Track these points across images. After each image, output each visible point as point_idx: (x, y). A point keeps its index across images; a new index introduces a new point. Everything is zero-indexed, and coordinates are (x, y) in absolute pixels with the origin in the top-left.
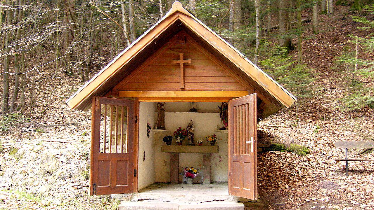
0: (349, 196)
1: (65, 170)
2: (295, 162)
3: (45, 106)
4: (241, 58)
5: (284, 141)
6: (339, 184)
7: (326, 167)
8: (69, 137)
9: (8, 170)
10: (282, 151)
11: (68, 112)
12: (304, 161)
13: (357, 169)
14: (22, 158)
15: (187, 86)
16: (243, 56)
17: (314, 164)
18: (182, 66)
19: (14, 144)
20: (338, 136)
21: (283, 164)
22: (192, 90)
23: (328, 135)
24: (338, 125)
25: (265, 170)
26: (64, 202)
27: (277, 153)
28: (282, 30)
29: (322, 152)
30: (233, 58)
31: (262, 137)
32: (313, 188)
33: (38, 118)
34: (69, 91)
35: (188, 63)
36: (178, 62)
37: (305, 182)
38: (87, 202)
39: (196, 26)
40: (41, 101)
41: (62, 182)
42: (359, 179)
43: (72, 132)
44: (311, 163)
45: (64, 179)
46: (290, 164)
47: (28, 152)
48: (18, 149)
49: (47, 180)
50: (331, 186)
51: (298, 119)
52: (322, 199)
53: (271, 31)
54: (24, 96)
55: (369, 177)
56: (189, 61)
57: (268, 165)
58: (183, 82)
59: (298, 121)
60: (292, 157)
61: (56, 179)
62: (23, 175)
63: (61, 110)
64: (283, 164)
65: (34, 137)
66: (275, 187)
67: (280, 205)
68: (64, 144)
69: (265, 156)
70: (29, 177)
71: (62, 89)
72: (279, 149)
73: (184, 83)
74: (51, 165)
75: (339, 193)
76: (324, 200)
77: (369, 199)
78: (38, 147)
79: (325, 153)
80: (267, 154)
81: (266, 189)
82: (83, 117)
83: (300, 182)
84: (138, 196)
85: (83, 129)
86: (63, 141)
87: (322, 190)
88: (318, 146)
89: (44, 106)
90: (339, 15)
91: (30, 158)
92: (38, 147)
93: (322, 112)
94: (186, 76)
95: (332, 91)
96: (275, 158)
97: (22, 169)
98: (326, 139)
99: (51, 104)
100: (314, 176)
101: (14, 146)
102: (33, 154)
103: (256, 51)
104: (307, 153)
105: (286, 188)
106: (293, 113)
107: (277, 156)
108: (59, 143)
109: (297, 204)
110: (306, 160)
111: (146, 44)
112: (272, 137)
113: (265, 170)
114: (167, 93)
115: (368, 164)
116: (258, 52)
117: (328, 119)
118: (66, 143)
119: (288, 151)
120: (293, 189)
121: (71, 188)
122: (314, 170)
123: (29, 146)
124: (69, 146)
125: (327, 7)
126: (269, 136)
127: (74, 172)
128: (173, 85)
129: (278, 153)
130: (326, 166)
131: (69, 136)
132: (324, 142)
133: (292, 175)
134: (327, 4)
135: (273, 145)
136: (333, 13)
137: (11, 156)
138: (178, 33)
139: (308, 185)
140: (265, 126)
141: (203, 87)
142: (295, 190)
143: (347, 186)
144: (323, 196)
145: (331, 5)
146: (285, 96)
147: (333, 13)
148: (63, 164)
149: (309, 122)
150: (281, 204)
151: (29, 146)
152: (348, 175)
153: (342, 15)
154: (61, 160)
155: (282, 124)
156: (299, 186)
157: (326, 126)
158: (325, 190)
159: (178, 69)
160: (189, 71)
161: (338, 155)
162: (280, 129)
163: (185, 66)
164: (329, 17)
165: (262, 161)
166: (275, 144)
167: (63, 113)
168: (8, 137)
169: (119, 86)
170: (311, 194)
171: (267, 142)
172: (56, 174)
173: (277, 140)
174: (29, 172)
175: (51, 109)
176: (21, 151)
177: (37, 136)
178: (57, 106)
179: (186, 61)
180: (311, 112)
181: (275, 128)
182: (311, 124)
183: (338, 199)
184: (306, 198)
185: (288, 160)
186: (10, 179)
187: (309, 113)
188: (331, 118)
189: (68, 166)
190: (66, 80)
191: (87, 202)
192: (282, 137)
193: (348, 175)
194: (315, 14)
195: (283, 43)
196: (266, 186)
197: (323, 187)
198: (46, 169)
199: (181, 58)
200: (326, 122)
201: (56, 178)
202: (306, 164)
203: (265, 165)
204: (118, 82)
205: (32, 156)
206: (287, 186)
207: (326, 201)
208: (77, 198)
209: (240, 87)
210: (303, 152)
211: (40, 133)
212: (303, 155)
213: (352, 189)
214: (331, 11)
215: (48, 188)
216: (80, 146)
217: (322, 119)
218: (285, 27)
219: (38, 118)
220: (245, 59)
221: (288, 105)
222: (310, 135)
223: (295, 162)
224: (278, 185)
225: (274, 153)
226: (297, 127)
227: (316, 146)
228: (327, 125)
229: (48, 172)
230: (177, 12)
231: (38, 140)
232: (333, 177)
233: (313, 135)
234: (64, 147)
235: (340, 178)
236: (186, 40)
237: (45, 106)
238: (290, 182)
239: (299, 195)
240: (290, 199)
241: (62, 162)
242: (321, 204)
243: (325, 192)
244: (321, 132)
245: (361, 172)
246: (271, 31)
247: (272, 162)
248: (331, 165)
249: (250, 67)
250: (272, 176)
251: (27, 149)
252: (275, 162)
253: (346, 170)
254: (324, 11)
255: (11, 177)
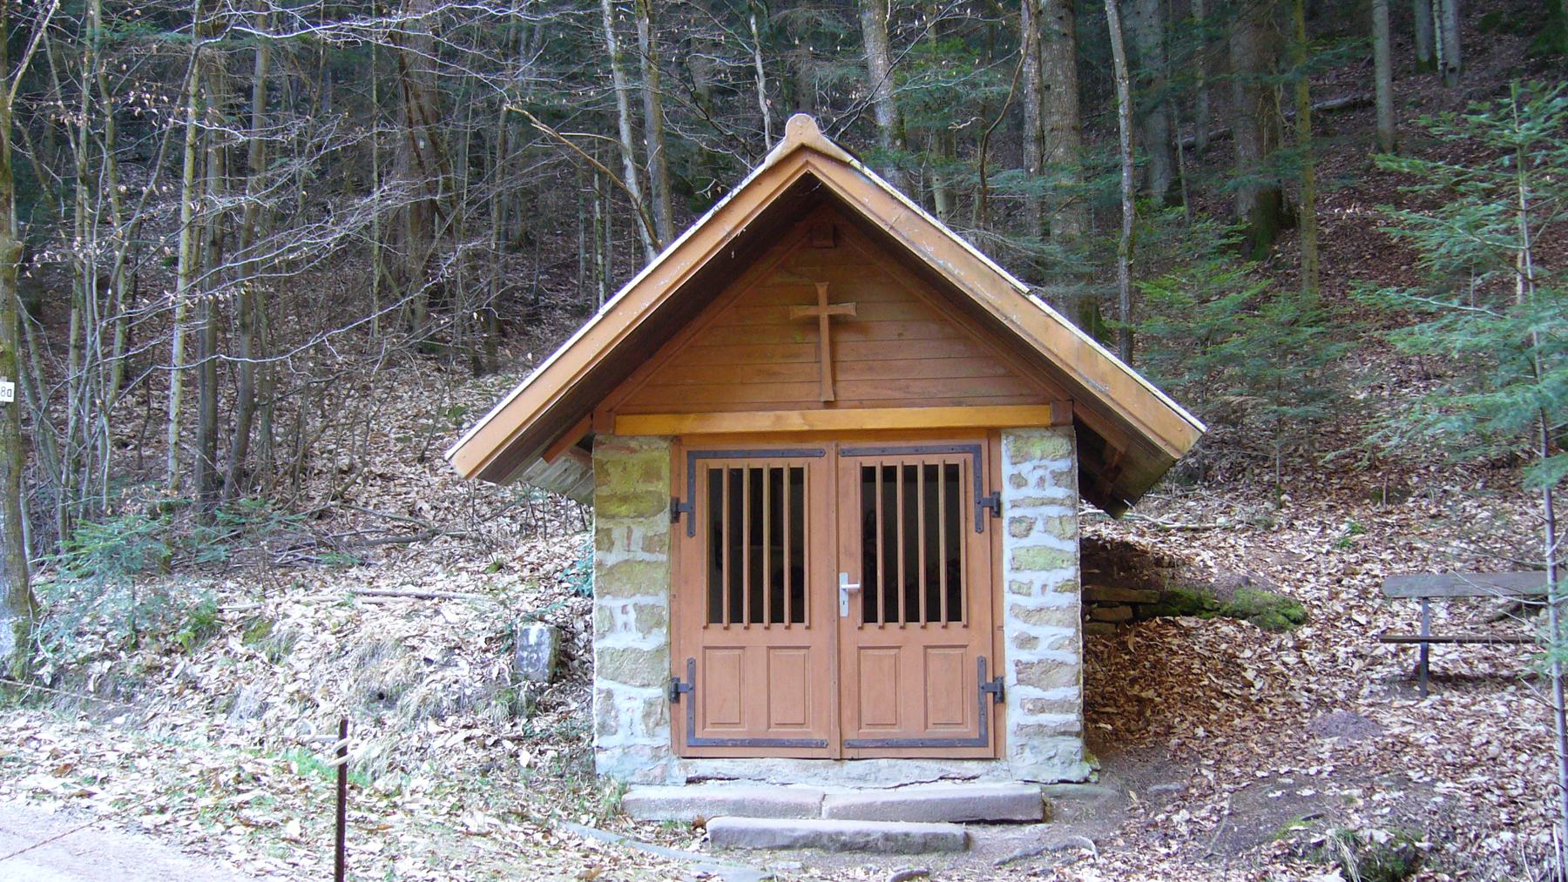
0: (1405, 759)
1: (440, 687)
2: (1248, 653)
3: (345, 472)
4: (1016, 296)
5: (1212, 580)
6: (1385, 722)
7: (1355, 669)
8: (440, 581)
9: (248, 691)
10: (1205, 614)
11: (428, 491)
12: (1280, 647)
13: (1465, 670)
14: (288, 650)
15: (843, 395)
16: (1024, 288)
17: (1313, 659)
18: (824, 325)
19: (256, 604)
20: (1425, 559)
21: (1204, 660)
22: (861, 404)
23: (1387, 556)
24: (1433, 517)
25: (1133, 681)
26: (447, 784)
27: (1184, 624)
28: (1245, 149)
29: (1355, 617)
30: (989, 296)
31: (1130, 568)
32: (1290, 737)
33: (321, 516)
34: (428, 415)
35: (845, 316)
36: (812, 311)
37: (1269, 716)
38: (520, 784)
39: (869, 192)
40: (330, 452)
41: (433, 727)
42: (1464, 706)
43: (448, 561)
44: (1305, 655)
45: (439, 717)
46: (1230, 659)
47: (308, 630)
48: (272, 622)
49: (379, 722)
50: (1351, 728)
51: (1284, 497)
52: (1312, 771)
53: (1208, 150)
54: (269, 439)
55: (1500, 699)
56: (847, 309)
57: (1148, 664)
58: (830, 381)
59: (1281, 505)
60: (1240, 636)
61: (411, 714)
62: (297, 708)
63: (404, 485)
64: (1204, 660)
65: (318, 584)
66: (1157, 734)
67: (1167, 791)
68: (428, 603)
69: (1139, 634)
70: (320, 711)
71: (399, 406)
72: (1195, 607)
73: (834, 382)
74: (392, 670)
75: (1372, 749)
76: (1319, 772)
77: (1473, 766)
78: (342, 614)
79: (1362, 620)
80: (1147, 628)
81: (1126, 744)
82: (485, 510)
83: (1250, 716)
84: (686, 767)
85: (490, 550)
86: (424, 591)
87: (1319, 741)
88: (1343, 596)
89: (342, 472)
90: (1484, 74)
91: (317, 651)
92: (342, 614)
93: (1377, 469)
94: (841, 357)
95: (1425, 388)
96: (1176, 641)
97: (294, 687)
98: (1377, 569)
99: (366, 464)
100: (1303, 698)
101: (257, 613)
102: (326, 637)
103: (1123, 247)
104: (1298, 622)
105: (1195, 737)
106: (1266, 478)
107: (1186, 633)
108: (411, 600)
109: (1225, 786)
110: (1291, 644)
111: (698, 263)
112: (1171, 565)
113: (1133, 681)
114: (779, 418)
115: (1514, 654)
116: (1131, 251)
117: (1397, 495)
118: (436, 600)
119: (1225, 614)
120: (1220, 740)
121: (462, 746)
122: (1312, 679)
123: (310, 611)
124: (445, 608)
125: (1439, 46)
126: (1159, 562)
127: (468, 692)
128: (797, 392)
129: (1186, 622)
130: (1358, 664)
131: (441, 576)
132: (1368, 581)
133: (1227, 696)
134: (1438, 32)
135: (1174, 596)
136: (1463, 69)
137: (251, 646)
138: (809, 213)
139: (1275, 726)
140: (1155, 525)
141: (898, 395)
142: (1225, 744)
143: (1408, 728)
144: (1318, 759)
145: (1451, 37)
146: (1167, 419)
147: (1463, 69)
148: (431, 668)
149: (1324, 507)
150: (1171, 787)
151: (310, 611)
152: (1426, 694)
153: (1497, 78)
154: (423, 653)
155: (1222, 520)
156: (1244, 729)
157: (1386, 524)
158: (1328, 743)
159: (812, 338)
160: (848, 340)
161: (1410, 625)
162: (1205, 538)
163: (836, 323)
164: (1445, 86)
165: (1129, 653)
166: (1177, 590)
167: (413, 495)
168: (229, 584)
169: (615, 399)
170: (1279, 754)
171: (1148, 584)
172: (412, 698)
173: (1188, 575)
174: (317, 696)
175: (366, 479)
176: (282, 628)
177: (329, 578)
178: (388, 471)
179: (838, 310)
180: (1336, 472)
181: (1189, 534)
182: (1329, 519)
183: (1368, 768)
184: (1258, 768)
185: (1224, 646)
186: (254, 721)
187: (1329, 476)
188: (1410, 494)
189: (450, 673)
190: (417, 366)
191: (520, 784)
192: (1206, 566)
193: (1428, 693)
194: (1382, 80)
195: (1252, 201)
196: (1128, 730)
197: (1326, 732)
198: (375, 685)
199: (823, 299)
200: (1389, 507)
201: (412, 711)
202: (1286, 659)
203: (1134, 663)
204: (617, 383)
205: (324, 645)
206: (1200, 732)
207: (1325, 775)
208: (485, 773)
209: (1026, 391)
210: (1281, 619)
211: (340, 568)
212: (1280, 629)
213: (1424, 736)
214: (1454, 61)
215: (387, 745)
216: (487, 606)
217: (1376, 496)
218: (1259, 139)
219: (321, 516)
220: (1033, 298)
221: (1177, 450)
222: (1321, 558)
223: (1248, 653)
224: (1170, 727)
225: (1175, 624)
226: (1275, 528)
227: (1334, 596)
228: (1392, 519)
229: (381, 696)
230: (803, 148)
231: (333, 592)
232: (1370, 700)
233: (1333, 559)
234: (428, 612)
235: (1396, 704)
236: (836, 235)
237: (345, 472)
238: (1213, 717)
239: (1236, 758)
240: (1204, 772)
241: (428, 661)
242: (1301, 786)
243: (1327, 747)
244: (1362, 543)
245: (1476, 681)
246: (1208, 150)
247: (1163, 655)
248: (1377, 661)
249: (1047, 328)
250: (1152, 700)
251: (301, 621)
252: (1176, 653)
253: (1423, 678)
254: (1425, 58)
255: (258, 714)
